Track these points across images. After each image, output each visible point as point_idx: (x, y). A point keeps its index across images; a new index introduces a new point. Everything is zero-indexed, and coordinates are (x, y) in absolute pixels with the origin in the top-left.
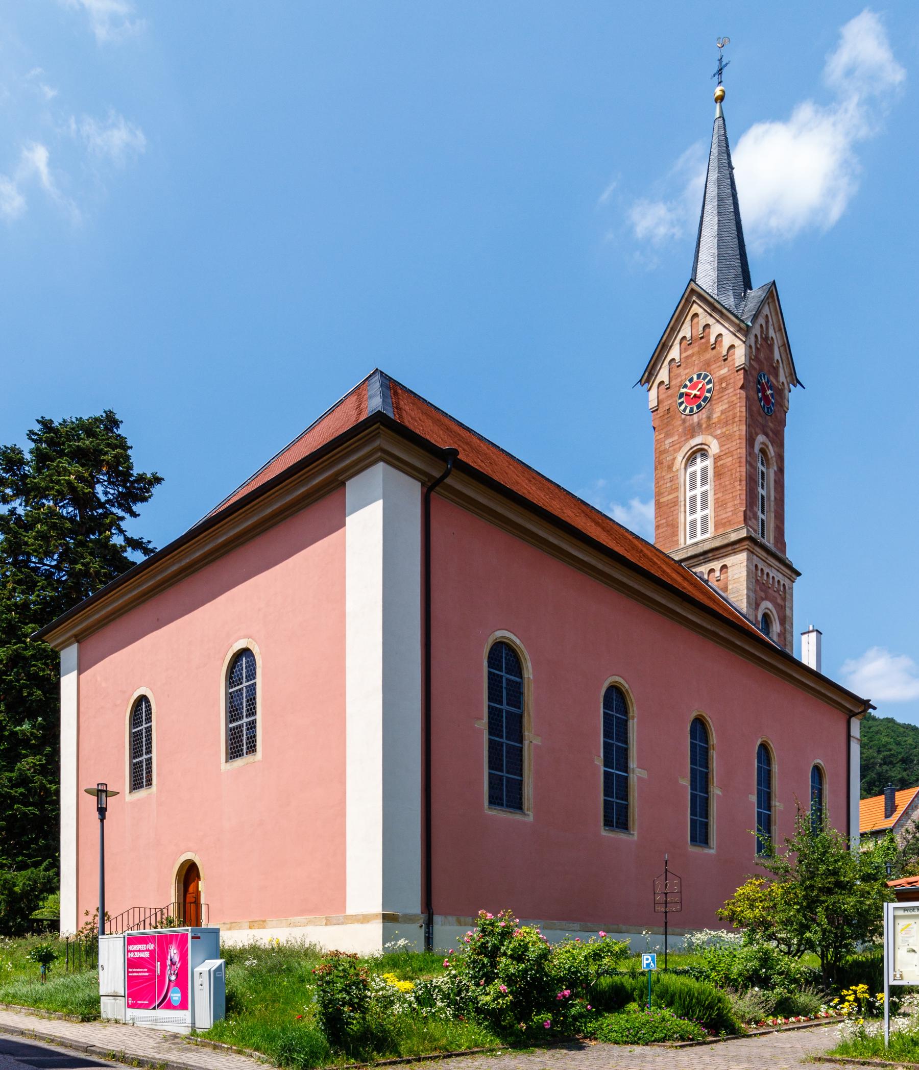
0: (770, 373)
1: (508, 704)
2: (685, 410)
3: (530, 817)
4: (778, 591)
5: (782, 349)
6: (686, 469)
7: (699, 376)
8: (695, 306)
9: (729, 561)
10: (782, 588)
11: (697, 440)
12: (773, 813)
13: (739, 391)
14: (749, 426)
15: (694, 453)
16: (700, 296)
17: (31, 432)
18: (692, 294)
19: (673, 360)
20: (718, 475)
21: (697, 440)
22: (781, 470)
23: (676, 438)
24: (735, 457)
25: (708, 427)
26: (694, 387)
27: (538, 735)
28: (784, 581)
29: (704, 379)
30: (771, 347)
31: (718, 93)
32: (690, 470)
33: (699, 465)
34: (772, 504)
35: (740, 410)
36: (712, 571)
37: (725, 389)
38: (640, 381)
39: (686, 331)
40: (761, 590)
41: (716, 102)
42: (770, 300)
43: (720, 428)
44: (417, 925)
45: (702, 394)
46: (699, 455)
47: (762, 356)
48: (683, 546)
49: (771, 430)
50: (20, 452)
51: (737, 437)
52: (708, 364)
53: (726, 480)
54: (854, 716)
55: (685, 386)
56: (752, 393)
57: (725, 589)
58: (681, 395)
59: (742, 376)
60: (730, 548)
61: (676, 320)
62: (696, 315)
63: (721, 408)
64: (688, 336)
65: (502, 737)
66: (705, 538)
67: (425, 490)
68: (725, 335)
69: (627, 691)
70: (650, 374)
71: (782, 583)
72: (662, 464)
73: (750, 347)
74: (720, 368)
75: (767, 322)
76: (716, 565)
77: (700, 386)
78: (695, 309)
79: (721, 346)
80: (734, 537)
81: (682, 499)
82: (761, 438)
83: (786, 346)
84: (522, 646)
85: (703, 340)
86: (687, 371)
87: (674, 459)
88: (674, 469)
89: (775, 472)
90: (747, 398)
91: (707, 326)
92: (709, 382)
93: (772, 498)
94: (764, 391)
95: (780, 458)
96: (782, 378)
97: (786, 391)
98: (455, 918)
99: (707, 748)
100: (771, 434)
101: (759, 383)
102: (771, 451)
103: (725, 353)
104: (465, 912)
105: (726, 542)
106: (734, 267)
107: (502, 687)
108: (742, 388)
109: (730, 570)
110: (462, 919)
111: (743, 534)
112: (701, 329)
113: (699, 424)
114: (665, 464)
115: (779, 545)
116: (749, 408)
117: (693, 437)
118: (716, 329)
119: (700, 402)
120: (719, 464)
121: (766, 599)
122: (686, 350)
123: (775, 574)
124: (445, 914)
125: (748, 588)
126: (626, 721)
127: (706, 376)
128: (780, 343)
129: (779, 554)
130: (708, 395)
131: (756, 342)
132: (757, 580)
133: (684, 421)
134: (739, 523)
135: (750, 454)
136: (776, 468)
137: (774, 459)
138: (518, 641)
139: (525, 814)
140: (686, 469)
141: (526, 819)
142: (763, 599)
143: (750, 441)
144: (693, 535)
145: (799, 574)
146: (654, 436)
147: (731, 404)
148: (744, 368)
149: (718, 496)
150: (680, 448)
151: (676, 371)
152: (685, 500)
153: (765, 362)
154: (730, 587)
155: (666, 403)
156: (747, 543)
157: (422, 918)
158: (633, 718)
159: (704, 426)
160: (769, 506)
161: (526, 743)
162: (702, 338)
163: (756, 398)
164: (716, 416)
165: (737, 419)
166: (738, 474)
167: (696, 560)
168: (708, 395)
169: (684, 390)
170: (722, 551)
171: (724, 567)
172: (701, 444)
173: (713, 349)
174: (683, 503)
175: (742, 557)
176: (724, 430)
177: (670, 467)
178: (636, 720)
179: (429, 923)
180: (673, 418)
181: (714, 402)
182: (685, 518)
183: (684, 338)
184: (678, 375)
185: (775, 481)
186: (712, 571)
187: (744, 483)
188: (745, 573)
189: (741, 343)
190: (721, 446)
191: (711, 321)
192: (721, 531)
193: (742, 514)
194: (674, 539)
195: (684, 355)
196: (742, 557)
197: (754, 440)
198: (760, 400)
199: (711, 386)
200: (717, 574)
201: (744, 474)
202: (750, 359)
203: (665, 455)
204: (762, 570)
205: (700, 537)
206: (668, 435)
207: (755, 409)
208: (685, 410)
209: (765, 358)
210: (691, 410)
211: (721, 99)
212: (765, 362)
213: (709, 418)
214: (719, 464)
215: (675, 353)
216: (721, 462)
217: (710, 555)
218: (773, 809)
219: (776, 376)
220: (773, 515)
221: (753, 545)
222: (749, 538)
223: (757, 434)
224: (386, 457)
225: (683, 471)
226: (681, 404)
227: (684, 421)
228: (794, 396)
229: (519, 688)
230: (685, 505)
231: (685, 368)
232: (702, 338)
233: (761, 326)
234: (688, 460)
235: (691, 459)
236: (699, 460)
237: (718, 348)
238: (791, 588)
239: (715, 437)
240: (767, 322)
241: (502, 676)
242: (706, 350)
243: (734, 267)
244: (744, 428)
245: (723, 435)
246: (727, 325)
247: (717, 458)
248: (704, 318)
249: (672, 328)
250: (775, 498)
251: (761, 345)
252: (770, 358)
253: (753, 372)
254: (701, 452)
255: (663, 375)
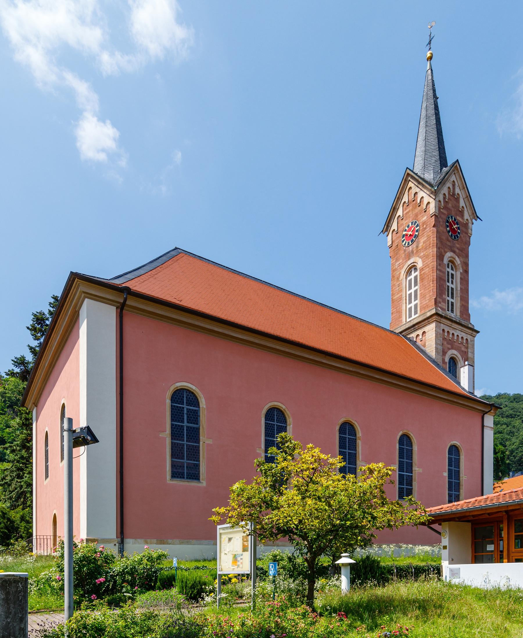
0: (456, 215)
1: (188, 422)
2: (405, 245)
3: (203, 483)
4: (462, 343)
5: (466, 200)
6: (406, 278)
7: (412, 223)
8: (410, 183)
9: (426, 329)
10: (465, 341)
11: (411, 261)
12: (413, 475)
13: (432, 229)
14: (438, 248)
15: (411, 268)
16: (412, 177)
17: (50, 303)
18: (409, 176)
19: (400, 216)
20: (422, 279)
21: (411, 261)
22: (466, 272)
23: (401, 261)
24: (430, 267)
25: (417, 252)
26: (409, 231)
27: (209, 438)
28: (469, 338)
29: (415, 225)
30: (457, 200)
31: (429, 55)
32: (409, 279)
33: (413, 275)
34: (459, 292)
35: (433, 239)
36: (418, 335)
37: (425, 228)
38: (382, 231)
39: (405, 199)
40: (448, 343)
41: (428, 61)
42: (456, 172)
43: (422, 252)
44: (113, 544)
45: (413, 234)
46: (413, 269)
47: (450, 205)
48: (404, 323)
49: (458, 248)
50: (44, 314)
51: (431, 256)
52: (416, 215)
53: (426, 282)
54: (486, 413)
55: (406, 230)
56: (442, 229)
57: (424, 346)
58: (403, 236)
59: (434, 220)
60: (426, 321)
61: (400, 193)
62: (410, 188)
63: (423, 240)
64: (407, 201)
65: (183, 440)
66: (415, 318)
67: (119, 310)
68: (425, 196)
69: (284, 410)
70: (388, 226)
71: (465, 338)
72: (395, 278)
73: (440, 201)
74: (423, 216)
75: (454, 185)
76: (420, 332)
77: (413, 229)
78: (410, 184)
79: (423, 204)
80: (429, 314)
81: (404, 296)
82: (449, 255)
83: (469, 197)
84: (197, 390)
85: (414, 202)
86: (407, 221)
87: (400, 273)
88: (400, 279)
89: (461, 273)
90: (437, 232)
91: (416, 193)
92: (417, 226)
93: (459, 289)
94: (451, 226)
95: (466, 265)
96: (466, 216)
97: (470, 225)
98: (143, 540)
99: (356, 439)
100: (457, 251)
101: (448, 222)
102: (458, 261)
103: (425, 207)
104: (146, 535)
105: (425, 317)
106: (434, 156)
107: (183, 413)
108: (434, 226)
109: (427, 334)
110: (149, 540)
111: (434, 311)
112: (413, 195)
113: (412, 251)
114: (396, 277)
115: (464, 316)
116: (439, 237)
117: (409, 259)
118: (421, 194)
119: (413, 238)
120: (422, 273)
121: (452, 348)
122: (406, 209)
123: (459, 333)
124: (135, 538)
125: (436, 343)
126: (286, 427)
127: (416, 222)
128: (464, 196)
129: (463, 322)
130: (417, 233)
131: (444, 198)
132: (444, 339)
133: (405, 251)
134: (432, 306)
135: (440, 265)
136: (461, 271)
137: (460, 266)
138: (194, 388)
139: (200, 482)
140: (406, 278)
141: (200, 485)
142: (449, 349)
143: (440, 257)
144: (410, 316)
145: (478, 332)
146: (392, 261)
147: (428, 237)
148: (435, 215)
149: (422, 291)
150: (403, 266)
151: (401, 222)
152: (406, 297)
153: (453, 209)
154: (427, 344)
155: (396, 242)
156: (435, 317)
157: (117, 541)
158: (290, 425)
159: (415, 252)
160: (457, 294)
161: (201, 443)
162: (413, 201)
163: (445, 230)
164: (421, 245)
165: (431, 245)
166: (432, 278)
167: (410, 330)
168: (417, 233)
169: (404, 233)
170: (422, 323)
171: (424, 332)
172: (413, 263)
173: (419, 206)
174: (404, 298)
175: (433, 326)
176: (425, 252)
177: (398, 279)
178: (291, 426)
179: (122, 543)
180: (399, 250)
181: (420, 237)
182: (405, 307)
183: (405, 202)
184: (402, 224)
185: (461, 278)
186: (418, 335)
187: (435, 282)
188: (434, 335)
189: (433, 200)
190: (423, 262)
191: (418, 190)
192: (423, 312)
193: (434, 300)
194: (400, 319)
195: (405, 212)
196: (433, 326)
197: (443, 256)
198: (449, 232)
199: (418, 228)
200: (420, 337)
201: (435, 277)
202: (440, 208)
203: (396, 272)
204: (448, 332)
205: (413, 317)
206: (397, 260)
207: (444, 238)
208: (405, 245)
209: (453, 207)
210: (408, 244)
211: (430, 58)
212: (453, 209)
213: (417, 247)
214: (422, 273)
215: (400, 212)
216: (423, 272)
217: (417, 326)
218: (414, 472)
219: (462, 216)
220: (459, 299)
221: (440, 318)
222: (437, 314)
223: (446, 252)
224: (87, 295)
225: (404, 280)
226: (403, 241)
227: (405, 251)
228: (476, 227)
229: (197, 413)
230: (406, 299)
231: (406, 220)
232: (413, 201)
233: (449, 188)
234: (407, 273)
235: (409, 272)
236: (413, 272)
237: (422, 205)
238: (474, 341)
239: (420, 257)
240: (454, 185)
241: (183, 408)
242: (415, 208)
243: (434, 156)
244: (435, 249)
245: (424, 256)
246: (425, 191)
247: (422, 269)
248: (415, 189)
249: (398, 198)
250: (461, 289)
251: (449, 199)
252: (457, 206)
253: (443, 216)
254: (413, 267)
255: (394, 226)
